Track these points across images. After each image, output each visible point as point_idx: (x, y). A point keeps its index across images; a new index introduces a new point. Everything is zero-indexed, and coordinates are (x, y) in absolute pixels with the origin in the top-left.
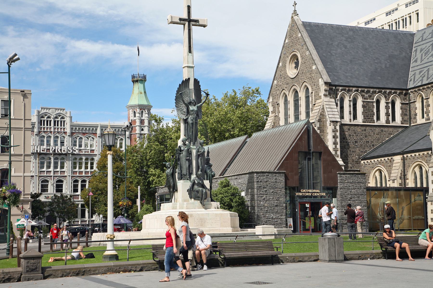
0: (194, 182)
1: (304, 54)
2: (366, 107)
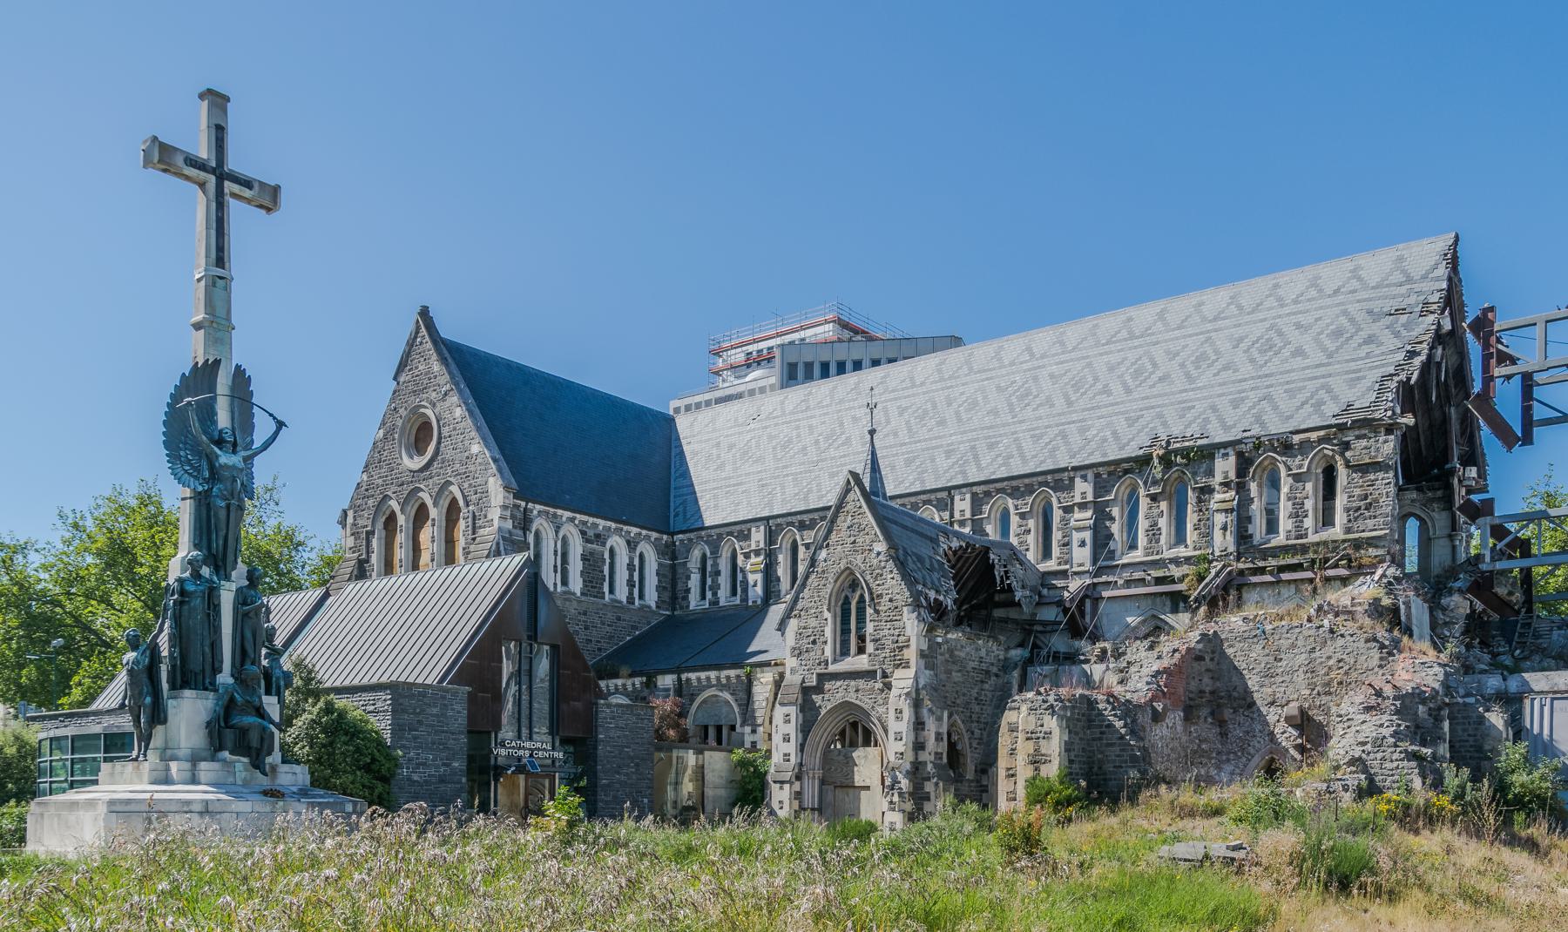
0: (232, 700)
2: (589, 560)
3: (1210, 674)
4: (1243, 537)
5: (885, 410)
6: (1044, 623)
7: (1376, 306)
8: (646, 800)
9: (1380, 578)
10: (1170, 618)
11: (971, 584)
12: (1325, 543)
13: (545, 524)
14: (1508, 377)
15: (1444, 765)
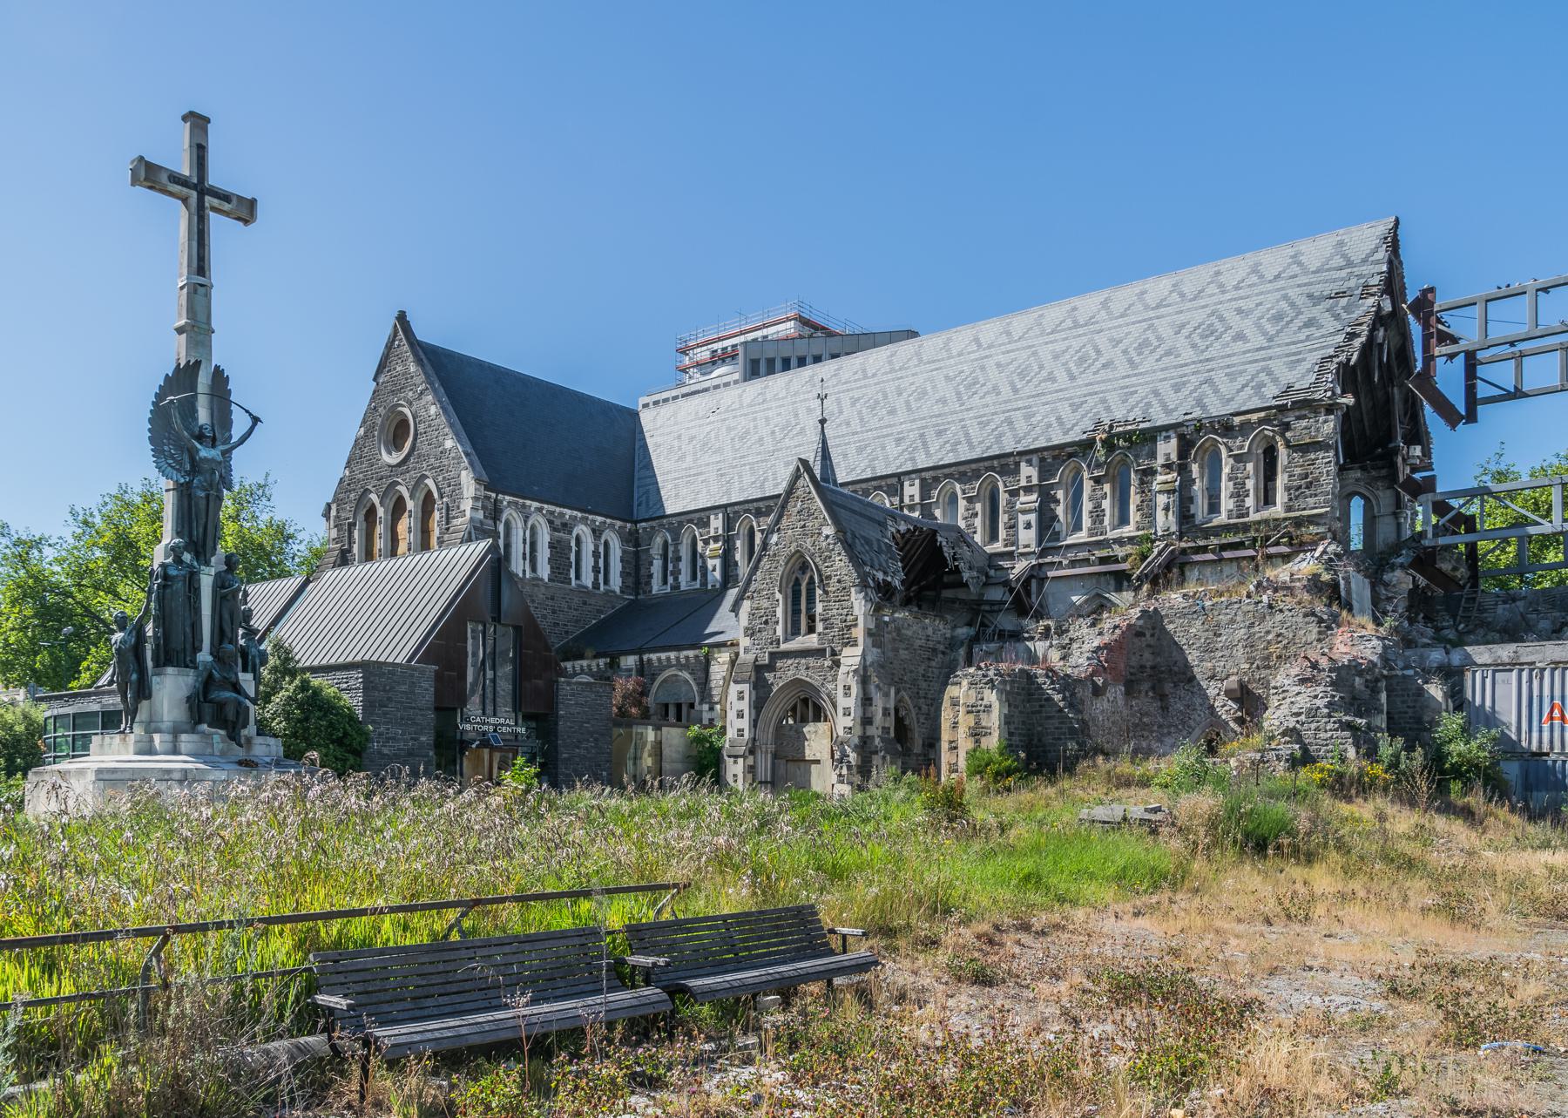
0: (210, 676)
3: (1151, 650)
4: (1185, 517)
5: (839, 401)
6: (992, 603)
7: (1316, 290)
8: (604, 773)
9: (1321, 555)
10: (1113, 597)
11: (920, 565)
12: (1266, 522)
13: (515, 515)
14: (1451, 356)
15: (1379, 735)
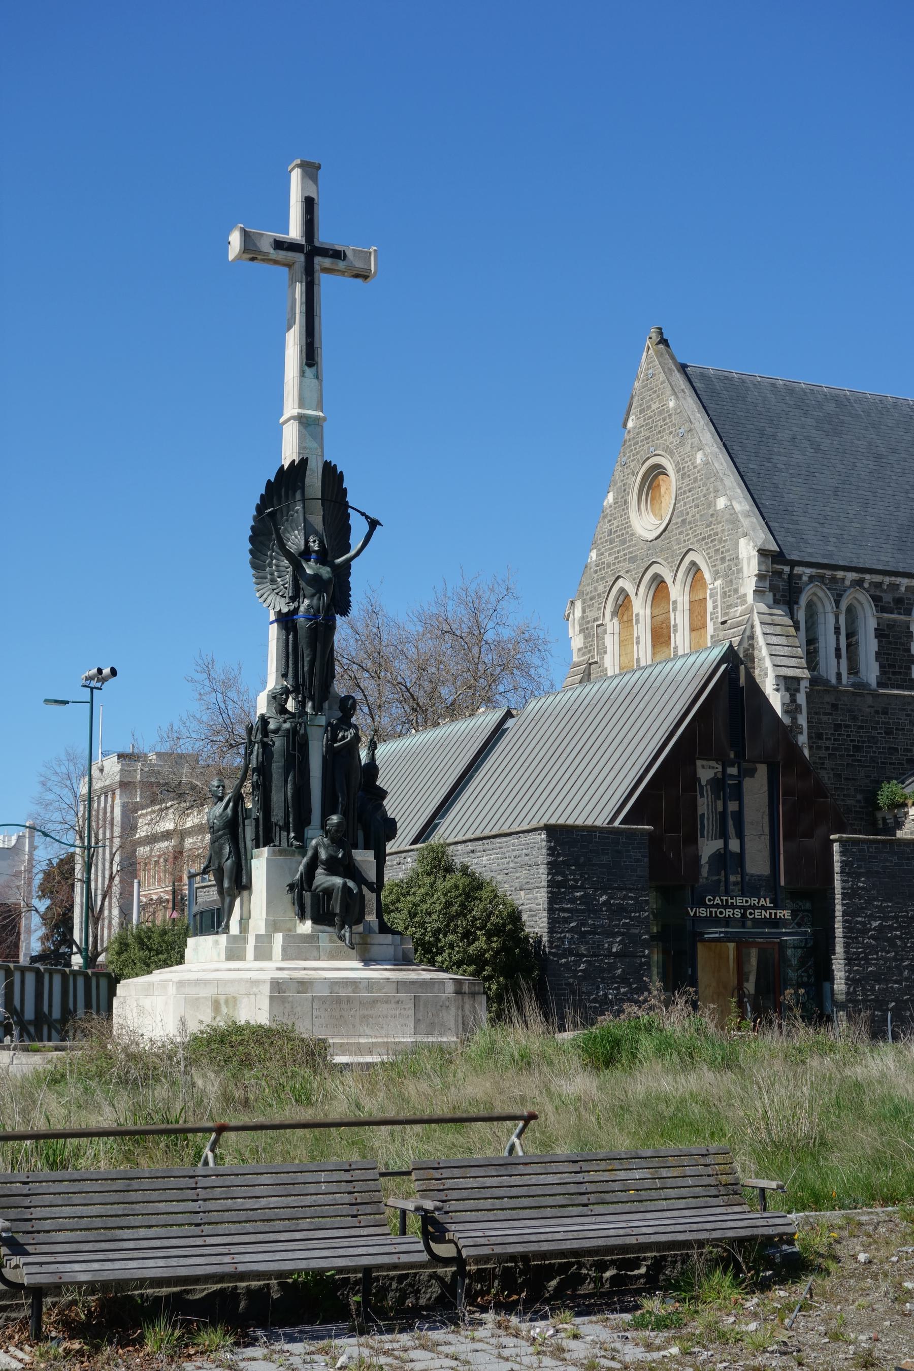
1: (689, 463)
2: (887, 636)
